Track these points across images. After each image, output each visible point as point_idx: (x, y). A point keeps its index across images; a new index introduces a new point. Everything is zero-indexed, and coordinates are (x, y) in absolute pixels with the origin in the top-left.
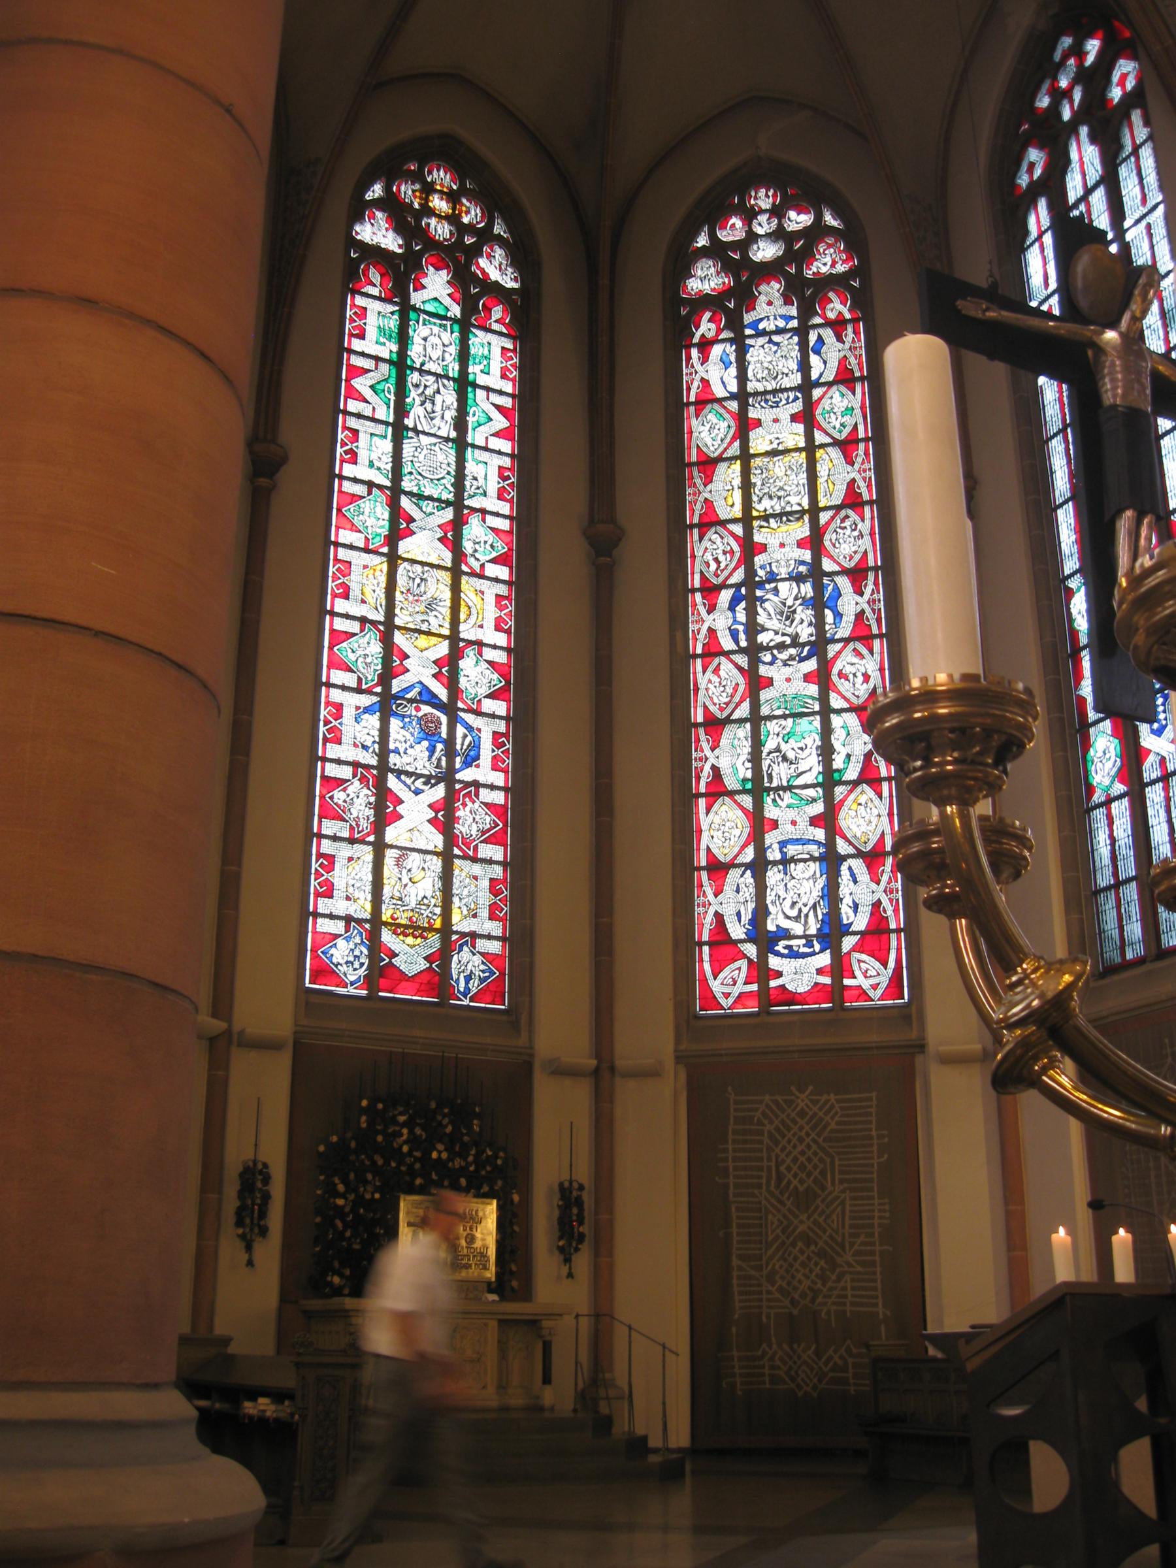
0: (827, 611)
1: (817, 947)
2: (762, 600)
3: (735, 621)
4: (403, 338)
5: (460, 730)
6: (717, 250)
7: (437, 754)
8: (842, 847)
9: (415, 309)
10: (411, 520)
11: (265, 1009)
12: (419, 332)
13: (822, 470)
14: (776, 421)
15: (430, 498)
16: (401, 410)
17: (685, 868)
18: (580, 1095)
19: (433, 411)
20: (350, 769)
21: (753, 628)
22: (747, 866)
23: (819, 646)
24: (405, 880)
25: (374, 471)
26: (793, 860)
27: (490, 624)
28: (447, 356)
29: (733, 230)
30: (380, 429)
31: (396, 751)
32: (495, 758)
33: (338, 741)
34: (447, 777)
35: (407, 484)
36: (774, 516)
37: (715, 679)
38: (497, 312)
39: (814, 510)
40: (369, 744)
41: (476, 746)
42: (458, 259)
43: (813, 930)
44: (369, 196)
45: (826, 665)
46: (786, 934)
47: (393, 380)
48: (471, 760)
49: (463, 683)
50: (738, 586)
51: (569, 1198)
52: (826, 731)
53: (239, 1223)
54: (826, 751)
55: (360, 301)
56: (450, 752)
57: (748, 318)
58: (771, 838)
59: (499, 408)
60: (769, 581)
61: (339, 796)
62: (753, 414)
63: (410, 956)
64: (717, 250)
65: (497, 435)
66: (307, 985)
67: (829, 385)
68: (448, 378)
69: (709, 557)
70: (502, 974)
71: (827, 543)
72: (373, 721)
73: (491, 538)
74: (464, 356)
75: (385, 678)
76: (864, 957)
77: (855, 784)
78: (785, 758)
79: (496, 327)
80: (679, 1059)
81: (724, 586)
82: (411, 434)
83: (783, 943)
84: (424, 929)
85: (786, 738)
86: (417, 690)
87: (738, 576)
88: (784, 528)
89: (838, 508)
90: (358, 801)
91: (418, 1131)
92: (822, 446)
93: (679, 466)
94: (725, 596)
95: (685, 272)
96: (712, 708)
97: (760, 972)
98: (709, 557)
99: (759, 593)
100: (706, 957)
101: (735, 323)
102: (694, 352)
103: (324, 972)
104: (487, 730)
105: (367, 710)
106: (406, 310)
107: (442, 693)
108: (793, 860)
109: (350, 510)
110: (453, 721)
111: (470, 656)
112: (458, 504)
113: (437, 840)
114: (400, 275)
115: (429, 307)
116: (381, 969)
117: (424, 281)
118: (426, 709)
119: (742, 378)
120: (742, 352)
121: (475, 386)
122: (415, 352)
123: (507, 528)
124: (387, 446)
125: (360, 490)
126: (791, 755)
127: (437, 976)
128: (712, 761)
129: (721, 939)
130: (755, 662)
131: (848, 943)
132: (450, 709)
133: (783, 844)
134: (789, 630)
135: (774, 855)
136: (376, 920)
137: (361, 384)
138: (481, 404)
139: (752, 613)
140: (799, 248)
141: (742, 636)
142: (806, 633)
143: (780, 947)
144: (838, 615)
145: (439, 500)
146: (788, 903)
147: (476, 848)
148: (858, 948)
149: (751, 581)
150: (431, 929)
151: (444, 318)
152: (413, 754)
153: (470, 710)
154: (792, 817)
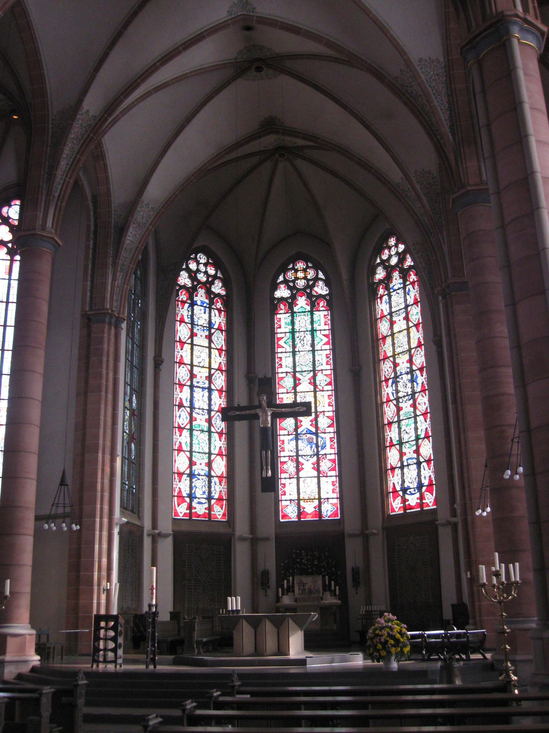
0: (415, 383)
1: (417, 491)
2: (399, 382)
3: (393, 390)
4: (293, 323)
5: (320, 439)
6: (286, 282)
7: (313, 448)
8: (421, 460)
9: (295, 312)
10: (300, 380)
11: (267, 529)
12: (297, 320)
13: (411, 335)
14: (399, 320)
15: (305, 371)
16: (294, 346)
17: (383, 471)
18: (359, 541)
19: (303, 345)
20: (288, 458)
21: (397, 392)
22: (399, 467)
23: (414, 393)
24: (306, 486)
25: (287, 368)
26: (410, 465)
27: (327, 405)
28: (307, 324)
29: (290, 275)
30: (288, 354)
31: (301, 450)
32: (331, 445)
33: (284, 451)
34: (317, 454)
35: (298, 369)
36: (400, 353)
37: (389, 409)
38: (321, 304)
39: (410, 350)
40: (292, 449)
41: (325, 443)
42: (308, 291)
43: (415, 486)
44: (279, 281)
45: (415, 401)
46: (409, 488)
47: (291, 338)
48: (323, 447)
49: (319, 425)
50: (393, 378)
51: (355, 571)
52: (416, 422)
53: (262, 585)
54: (416, 429)
55: (278, 316)
56: (317, 446)
57: (391, 285)
58: (405, 458)
59: (324, 335)
60: (400, 375)
61: (285, 466)
62: (394, 319)
63: (309, 508)
64: (383, 262)
65: (324, 344)
66: (281, 520)
67: (412, 305)
68: (307, 331)
69: (386, 370)
70: (337, 508)
71: (414, 360)
72: (294, 443)
73: (325, 378)
74: (312, 322)
75: (296, 430)
76: (427, 493)
77: (424, 438)
78: (407, 433)
79: (322, 309)
80: (383, 528)
81: (390, 378)
82: (298, 353)
83: (409, 491)
84: (313, 499)
85: (407, 425)
86: (306, 430)
87: (393, 376)
88: (403, 357)
89: (416, 348)
90: (291, 467)
91: (309, 557)
92: (411, 327)
93: (376, 341)
94: (390, 381)
95: (374, 273)
96: (389, 419)
97: (190, 507)
98: (386, 370)
99: (398, 380)
100: (391, 497)
101: (387, 288)
102: (379, 300)
103: (285, 516)
104: (327, 437)
105: (291, 440)
106: (293, 313)
107: (314, 430)
108: (410, 465)
109: (281, 383)
110: (317, 436)
111: (321, 416)
112: (314, 370)
113: (315, 473)
114: (290, 303)
115: (300, 311)
116: (301, 513)
117: (297, 303)
118: (309, 435)
119: (391, 307)
120: (390, 297)
121: (316, 330)
122: (297, 327)
123: (330, 373)
124: (291, 359)
125: (284, 375)
126: (408, 432)
127: (319, 512)
128: (390, 436)
129: (395, 491)
130: (398, 402)
131: (424, 489)
132: (316, 434)
133: (407, 460)
134: (406, 391)
135: (405, 464)
136: (299, 500)
137: (281, 343)
138: (319, 335)
139: (397, 386)
140: (402, 260)
141: (395, 395)
142: (410, 391)
143: (408, 492)
144: (417, 384)
145: (308, 371)
146: (409, 478)
147: (327, 473)
148: (426, 491)
149: (396, 377)
150: (315, 499)
151: (305, 312)
152: (306, 449)
153: (322, 433)
154: (409, 450)
